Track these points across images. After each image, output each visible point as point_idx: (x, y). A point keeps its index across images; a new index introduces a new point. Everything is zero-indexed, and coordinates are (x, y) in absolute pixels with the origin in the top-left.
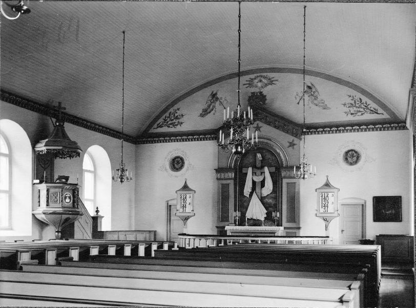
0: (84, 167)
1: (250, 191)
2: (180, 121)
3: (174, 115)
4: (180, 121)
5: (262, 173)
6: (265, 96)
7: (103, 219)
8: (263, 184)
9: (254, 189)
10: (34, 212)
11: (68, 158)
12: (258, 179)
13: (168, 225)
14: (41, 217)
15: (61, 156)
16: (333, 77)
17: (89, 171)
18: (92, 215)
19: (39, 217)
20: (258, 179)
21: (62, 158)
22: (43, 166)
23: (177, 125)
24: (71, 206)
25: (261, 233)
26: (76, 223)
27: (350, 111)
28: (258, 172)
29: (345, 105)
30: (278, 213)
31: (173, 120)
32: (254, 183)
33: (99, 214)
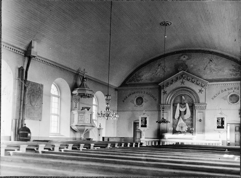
0: (93, 103)
1: (178, 116)
2: (141, 78)
3: (138, 75)
4: (141, 78)
5: (184, 107)
6: (78, 71)
7: (103, 130)
8: (185, 112)
9: (180, 115)
10: (72, 125)
11: (87, 98)
12: (183, 110)
13: (23, 92)
14: (75, 128)
15: (84, 97)
16: (19, 74)
17: (55, 96)
18: (98, 128)
19: (73, 128)
20: (183, 110)
21: (84, 98)
22: (75, 101)
23: (139, 81)
24: (89, 123)
25: (216, 148)
26: (90, 132)
27: (233, 74)
28: (183, 106)
29: (230, 70)
30: (193, 128)
31: (137, 78)
32: (180, 112)
33: (101, 127)
